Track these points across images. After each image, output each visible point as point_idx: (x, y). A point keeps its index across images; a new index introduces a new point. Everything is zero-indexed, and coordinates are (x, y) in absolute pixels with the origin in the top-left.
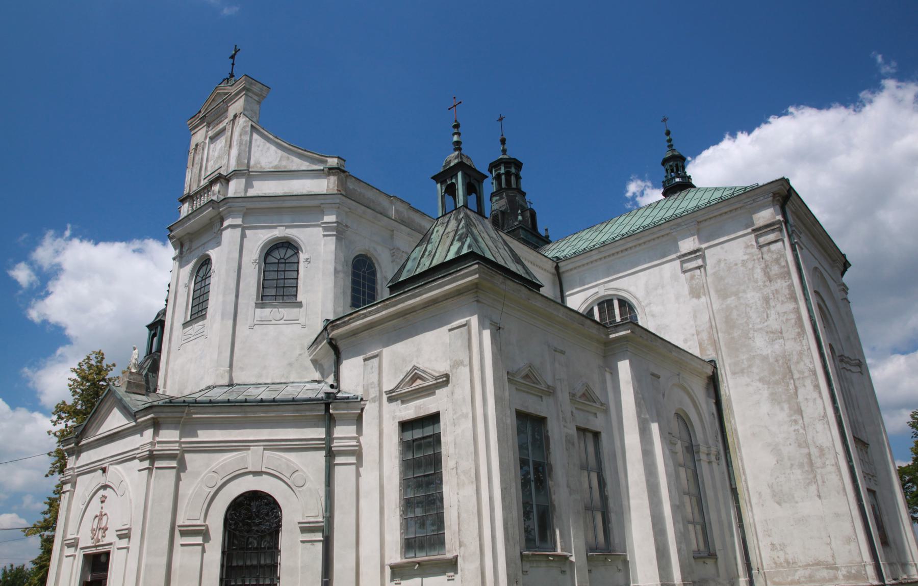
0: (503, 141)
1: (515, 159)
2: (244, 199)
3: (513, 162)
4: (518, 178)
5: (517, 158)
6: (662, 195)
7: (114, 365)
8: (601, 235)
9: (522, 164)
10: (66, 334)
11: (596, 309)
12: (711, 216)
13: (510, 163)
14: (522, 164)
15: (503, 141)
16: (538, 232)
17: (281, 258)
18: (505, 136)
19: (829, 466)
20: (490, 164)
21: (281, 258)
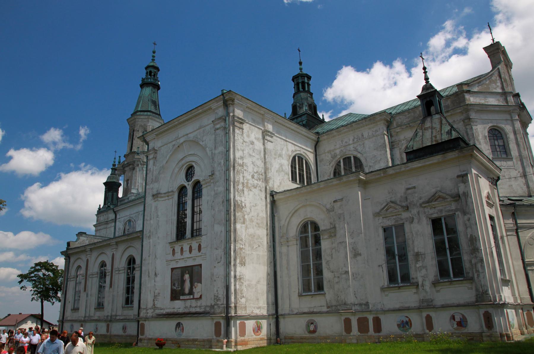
0: (300, 63)
1: (306, 74)
2: (479, 106)
3: (306, 76)
4: (309, 85)
5: (308, 74)
6: (139, 86)
7: (190, 171)
8: (343, 122)
9: (311, 77)
10: (12, 150)
11: (342, 161)
12: (253, 108)
13: (304, 76)
14: (311, 77)
15: (300, 63)
16: (526, 130)
17: (495, 134)
18: (302, 61)
19: (41, 272)
20: (293, 77)
21: (495, 134)
